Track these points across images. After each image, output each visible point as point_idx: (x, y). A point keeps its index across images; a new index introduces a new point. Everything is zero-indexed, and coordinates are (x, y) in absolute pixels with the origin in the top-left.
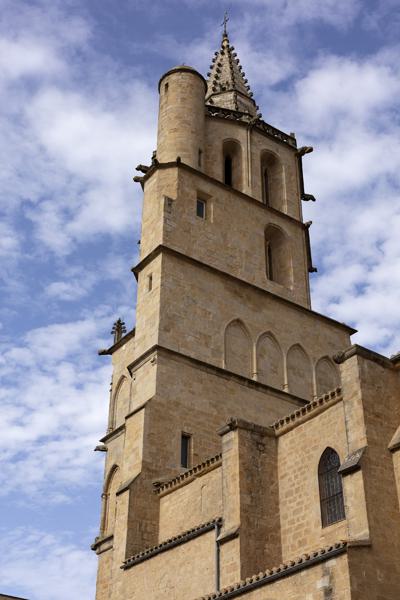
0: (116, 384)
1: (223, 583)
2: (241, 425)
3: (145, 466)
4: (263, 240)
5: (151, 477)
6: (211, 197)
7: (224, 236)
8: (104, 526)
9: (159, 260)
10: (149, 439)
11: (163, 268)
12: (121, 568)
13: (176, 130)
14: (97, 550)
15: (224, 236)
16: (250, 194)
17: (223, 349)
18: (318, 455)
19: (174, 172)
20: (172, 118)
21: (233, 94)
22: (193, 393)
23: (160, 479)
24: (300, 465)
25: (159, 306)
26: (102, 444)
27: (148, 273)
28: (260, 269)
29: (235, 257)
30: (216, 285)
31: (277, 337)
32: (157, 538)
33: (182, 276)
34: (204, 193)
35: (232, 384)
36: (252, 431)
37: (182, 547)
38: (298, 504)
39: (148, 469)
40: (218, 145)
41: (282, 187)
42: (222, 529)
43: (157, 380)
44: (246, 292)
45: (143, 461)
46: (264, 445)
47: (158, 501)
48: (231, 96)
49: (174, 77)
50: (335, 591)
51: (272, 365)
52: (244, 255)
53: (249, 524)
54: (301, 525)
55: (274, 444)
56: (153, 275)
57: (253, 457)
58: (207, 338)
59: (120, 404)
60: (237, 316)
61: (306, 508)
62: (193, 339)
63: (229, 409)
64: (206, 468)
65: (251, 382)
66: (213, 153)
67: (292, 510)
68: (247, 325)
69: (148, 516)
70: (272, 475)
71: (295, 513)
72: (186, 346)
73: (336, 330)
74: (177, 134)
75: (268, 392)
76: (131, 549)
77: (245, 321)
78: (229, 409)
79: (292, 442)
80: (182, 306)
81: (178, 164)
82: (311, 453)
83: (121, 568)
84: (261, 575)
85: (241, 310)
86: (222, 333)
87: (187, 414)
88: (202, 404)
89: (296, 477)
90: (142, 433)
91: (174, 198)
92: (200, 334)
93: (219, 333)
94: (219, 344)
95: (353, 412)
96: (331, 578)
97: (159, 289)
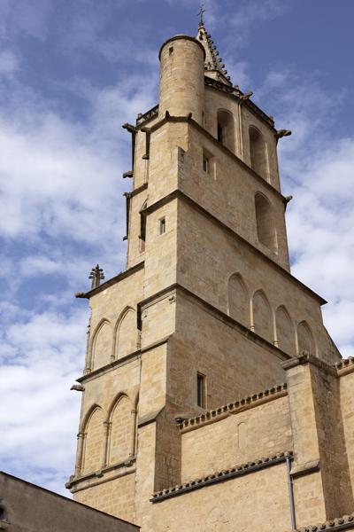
0: (94, 326)
2: (312, 360)
3: (169, 400)
6: (213, 156)
7: (225, 194)
8: (80, 465)
9: (174, 204)
10: (172, 374)
11: (179, 213)
12: (151, 500)
13: (182, 90)
14: (73, 489)
15: (225, 194)
16: (241, 157)
17: (227, 298)
19: (184, 127)
20: (179, 79)
22: (205, 336)
23: (181, 415)
25: (175, 247)
26: (79, 384)
27: (161, 216)
28: (253, 231)
29: (233, 216)
30: (219, 237)
31: (268, 295)
32: (178, 467)
33: (194, 223)
34: (208, 152)
35: (235, 332)
36: (320, 367)
37: (237, 480)
40: (214, 113)
41: (265, 162)
42: (294, 463)
43: (176, 317)
44: (244, 249)
45: (167, 396)
46: (329, 383)
47: (179, 437)
49: (179, 43)
51: (263, 321)
52: (240, 215)
53: (327, 459)
55: (336, 384)
57: (323, 394)
59: (99, 346)
60: (238, 270)
62: (204, 284)
63: (234, 357)
64: (246, 405)
65: (244, 329)
66: (210, 119)
68: (245, 282)
69: (172, 451)
70: (337, 413)
72: (198, 290)
73: (311, 299)
74: (184, 94)
75: (264, 346)
76: (159, 485)
81: (188, 119)
83: (151, 500)
84: (346, 518)
85: (240, 266)
86: (226, 283)
87: (201, 355)
88: (212, 347)
90: (164, 367)
91: (186, 150)
92: (209, 280)
93: (223, 282)
94: (224, 293)
97: (175, 232)
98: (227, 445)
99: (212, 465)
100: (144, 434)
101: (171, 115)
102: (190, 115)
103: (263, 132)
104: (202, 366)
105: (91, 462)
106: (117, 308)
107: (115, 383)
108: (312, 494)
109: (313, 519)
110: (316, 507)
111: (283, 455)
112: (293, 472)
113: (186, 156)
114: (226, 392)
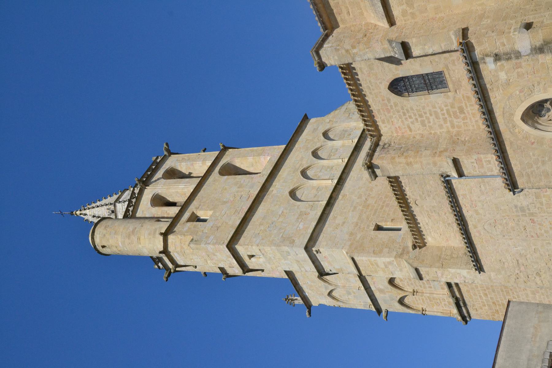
1: (492, 171)
4: (230, 177)
5: (408, 252)
7: (225, 203)
14: (468, 319)
15: (225, 203)
18: (394, 98)
19: (171, 238)
21: (117, 204)
22: (344, 223)
24: (402, 114)
31: (305, 166)
38: (431, 115)
39: (402, 254)
48: (119, 206)
50: (496, 51)
52: (241, 189)
54: (448, 111)
56: (249, 254)
58: (301, 214)
61: (434, 107)
62: (302, 223)
63: (358, 198)
67: (436, 120)
71: (437, 117)
74: (142, 237)
77: (291, 188)
78: (358, 198)
79: (383, 122)
80: (275, 231)
81: (165, 235)
82: (392, 104)
89: (410, 117)
92: (298, 218)
94: (307, 205)
95: (361, 53)
96: (487, 55)
98: (434, 214)
99: (449, 224)
100: (427, 276)
101: (162, 249)
102: (161, 234)
103: (168, 167)
104: (368, 226)
105: (445, 305)
106: (320, 285)
107: (381, 287)
108: (473, 163)
109: (492, 162)
110: (483, 160)
111: (443, 181)
112: (456, 176)
113: (195, 238)
114: (387, 205)
